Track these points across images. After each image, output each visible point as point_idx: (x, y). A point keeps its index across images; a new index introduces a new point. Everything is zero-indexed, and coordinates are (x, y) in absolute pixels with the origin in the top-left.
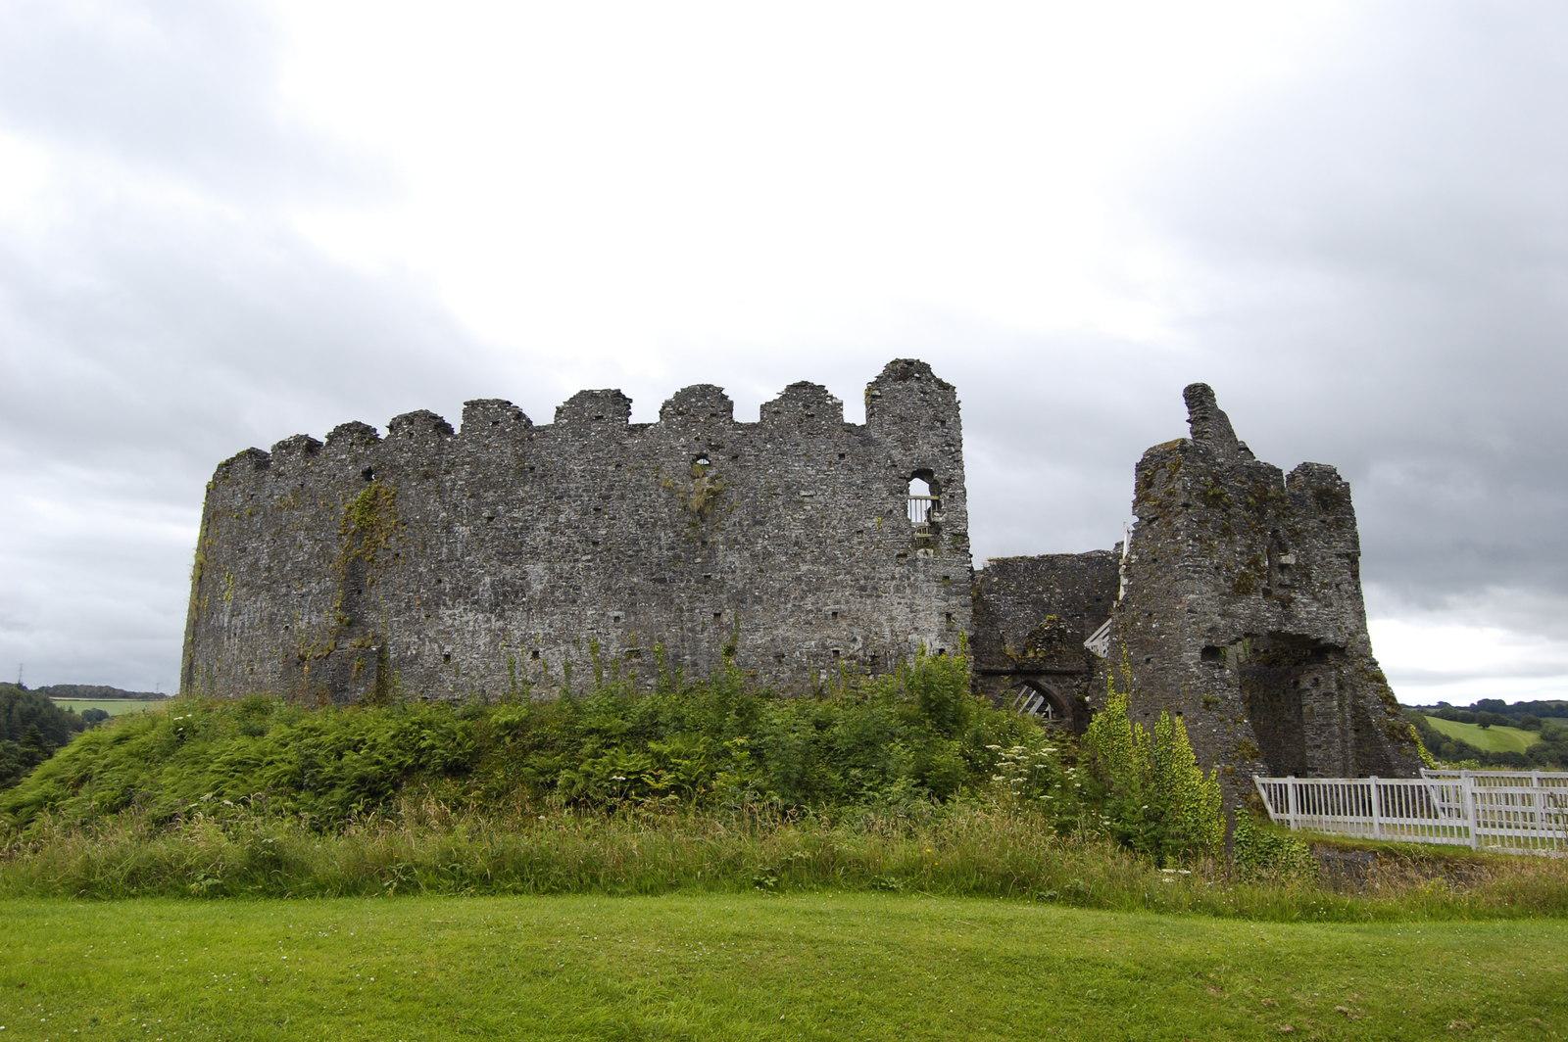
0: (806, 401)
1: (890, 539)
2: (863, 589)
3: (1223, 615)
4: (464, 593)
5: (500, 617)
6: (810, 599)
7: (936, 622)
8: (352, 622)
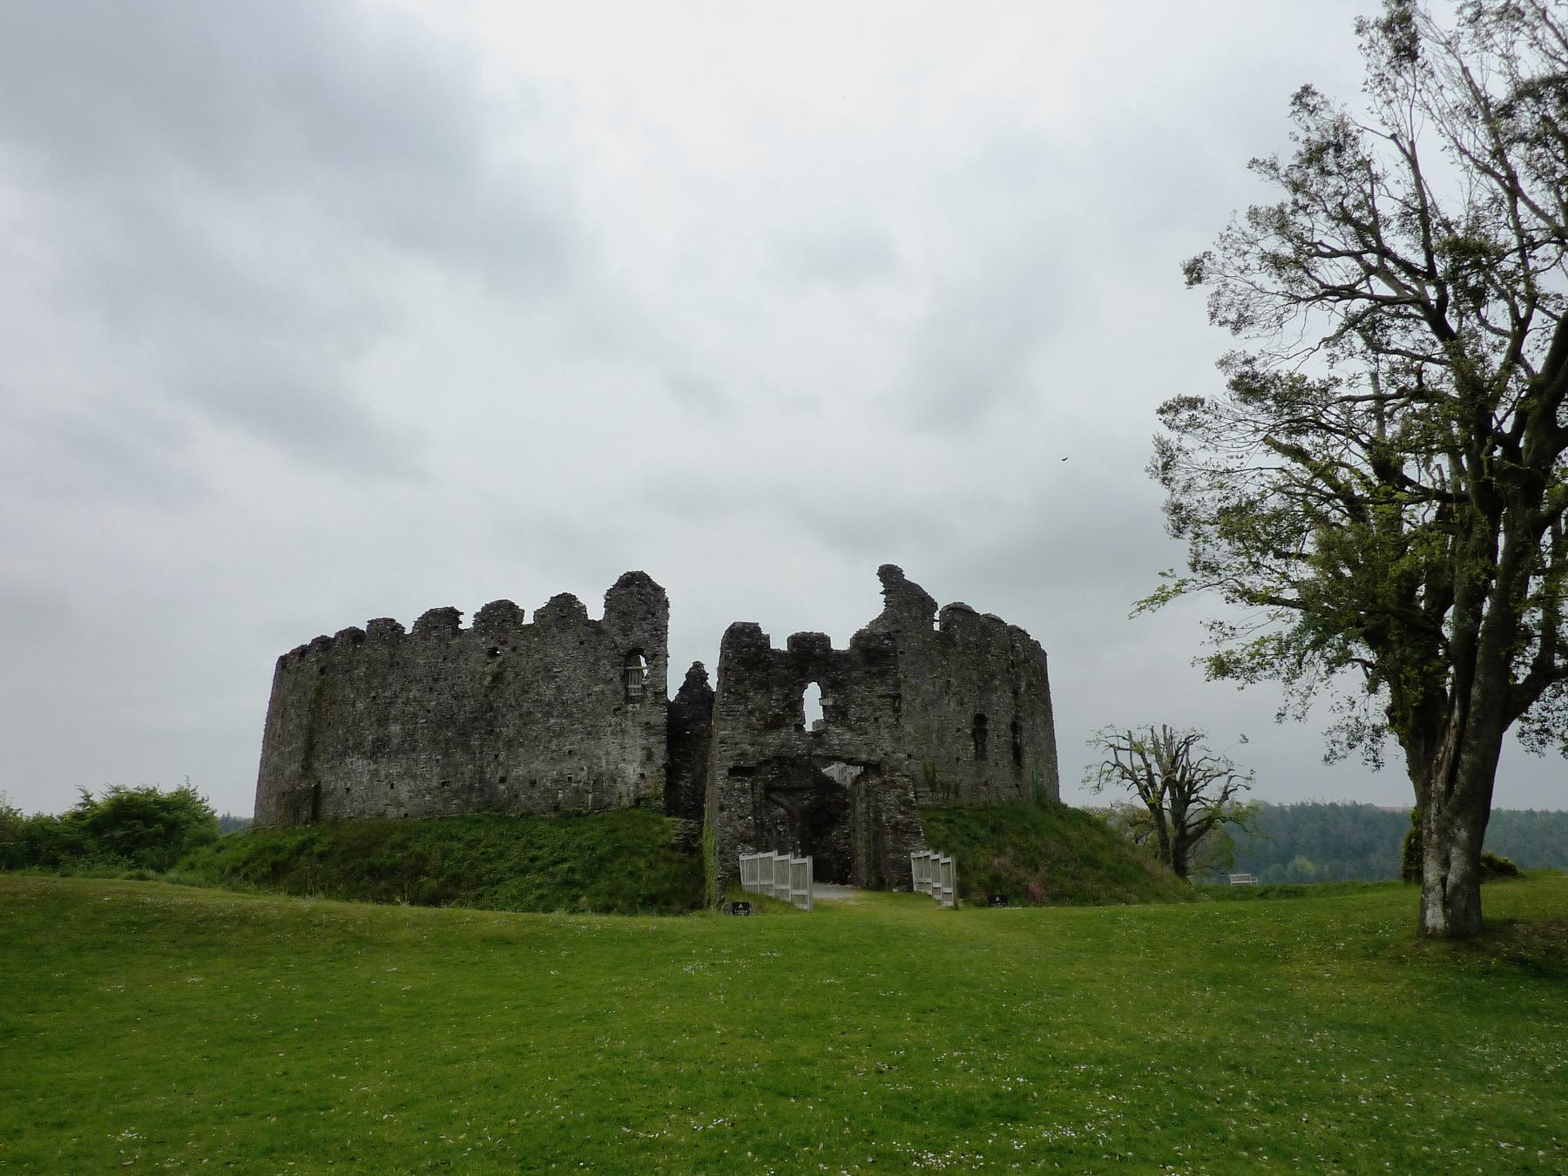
0: (564, 608)
1: (610, 697)
2: (589, 733)
3: (752, 745)
4: (357, 747)
5: (376, 762)
6: (555, 742)
7: (639, 754)
8: (307, 768)
